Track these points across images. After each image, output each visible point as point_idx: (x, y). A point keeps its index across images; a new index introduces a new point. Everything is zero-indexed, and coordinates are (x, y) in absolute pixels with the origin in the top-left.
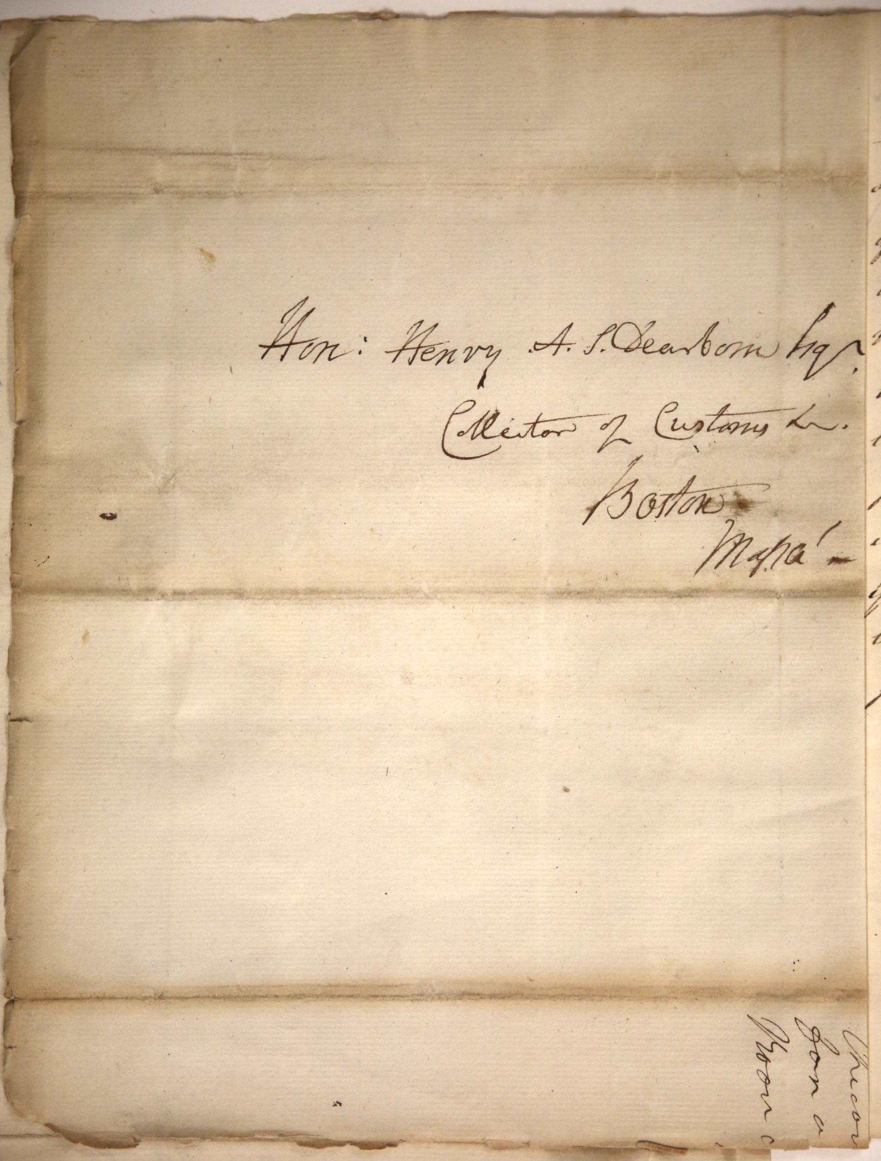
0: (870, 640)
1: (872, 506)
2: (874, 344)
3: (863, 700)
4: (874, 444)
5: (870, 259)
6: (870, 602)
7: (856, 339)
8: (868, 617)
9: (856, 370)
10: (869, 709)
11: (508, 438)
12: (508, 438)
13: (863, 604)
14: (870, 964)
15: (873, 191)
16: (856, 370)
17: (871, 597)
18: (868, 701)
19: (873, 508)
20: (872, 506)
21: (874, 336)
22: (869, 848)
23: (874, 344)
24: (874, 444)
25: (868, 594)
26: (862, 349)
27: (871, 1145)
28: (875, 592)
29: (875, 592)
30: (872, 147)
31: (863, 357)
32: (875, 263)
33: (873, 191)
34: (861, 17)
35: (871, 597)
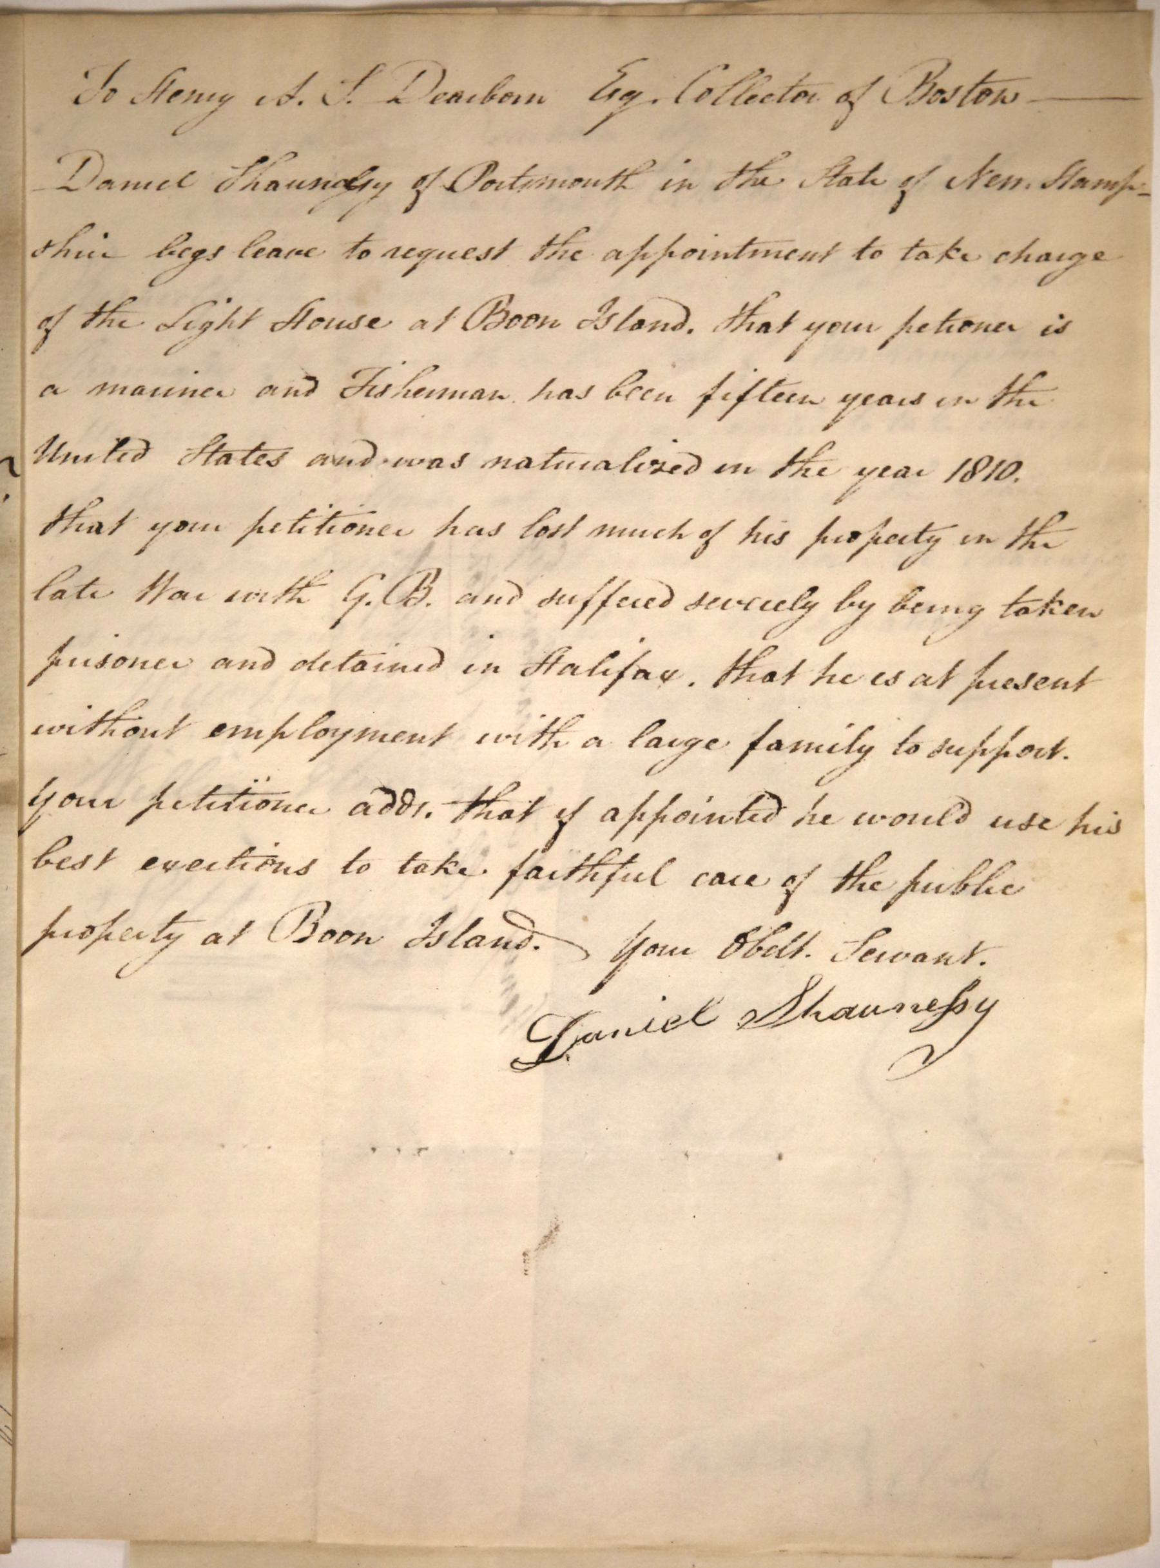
0: (28, 864)
1: (33, 680)
2: (35, 462)
3: (15, 946)
4: (36, 598)
5: (30, 346)
6: (28, 811)
7: (888, 393)
8: (26, 834)
9: (7, 496)
10: (26, 956)
11: (509, 922)
12: (509, 922)
13: (16, 813)
14: (21, 1302)
15: (34, 255)
16: (7, 496)
17: (31, 804)
18: (25, 946)
19: (35, 684)
20: (33, 680)
21: (36, 452)
22: (22, 1146)
23: (35, 462)
24: (36, 598)
25: (27, 800)
26: (17, 468)
27: (14, 1548)
28: (37, 797)
29: (37, 797)
30: (30, 198)
31: (18, 479)
32: (37, 353)
33: (34, 255)
34: (18, 19)
35: (31, 804)
